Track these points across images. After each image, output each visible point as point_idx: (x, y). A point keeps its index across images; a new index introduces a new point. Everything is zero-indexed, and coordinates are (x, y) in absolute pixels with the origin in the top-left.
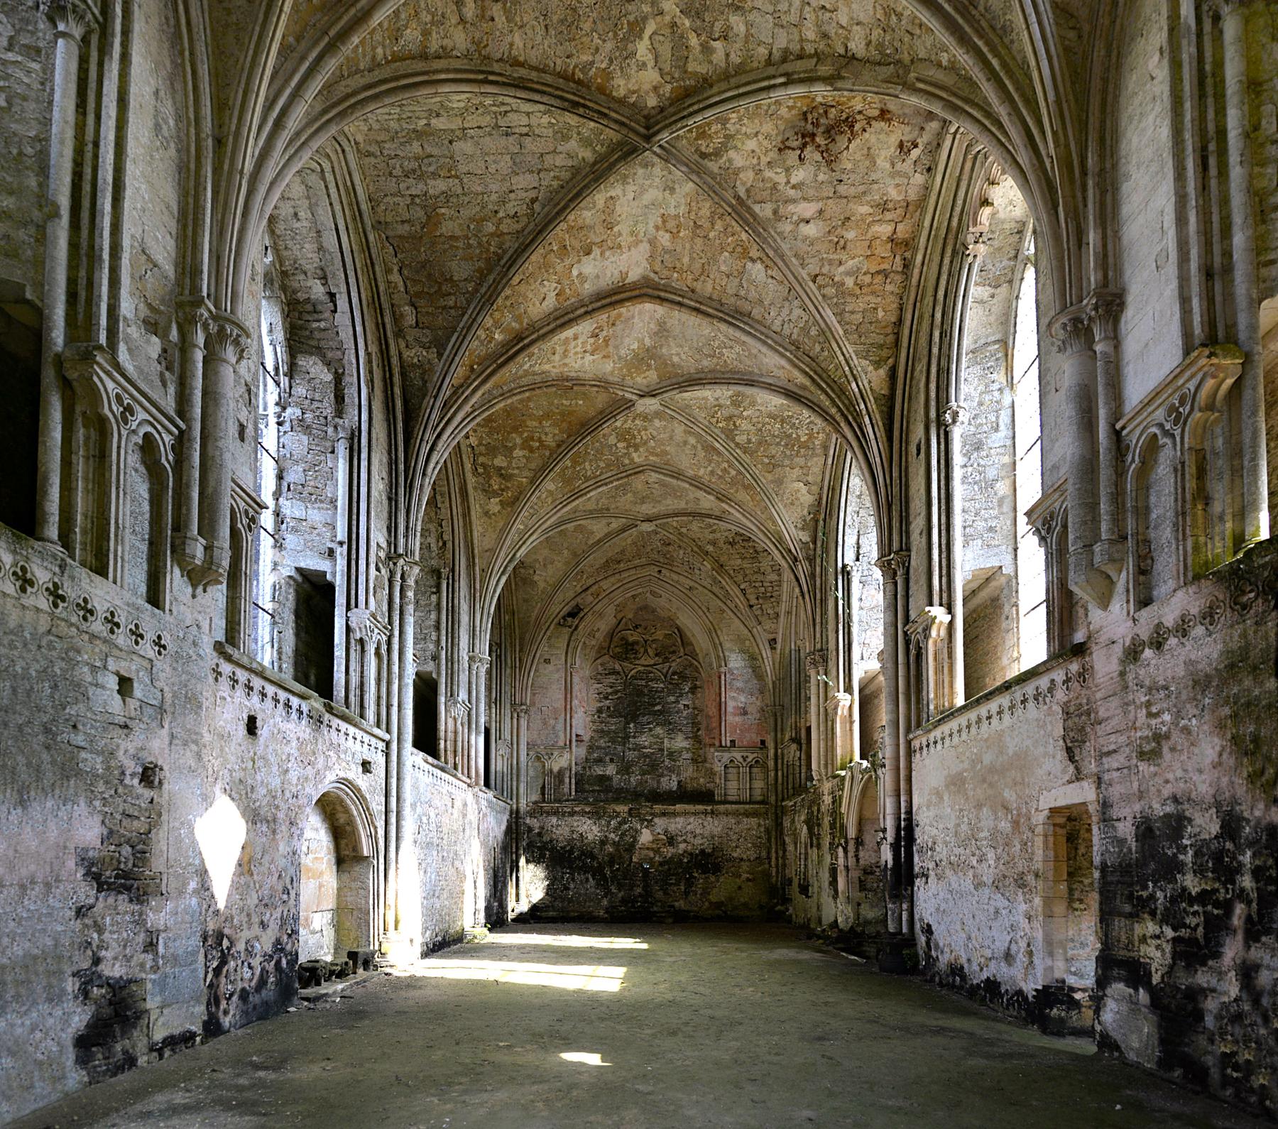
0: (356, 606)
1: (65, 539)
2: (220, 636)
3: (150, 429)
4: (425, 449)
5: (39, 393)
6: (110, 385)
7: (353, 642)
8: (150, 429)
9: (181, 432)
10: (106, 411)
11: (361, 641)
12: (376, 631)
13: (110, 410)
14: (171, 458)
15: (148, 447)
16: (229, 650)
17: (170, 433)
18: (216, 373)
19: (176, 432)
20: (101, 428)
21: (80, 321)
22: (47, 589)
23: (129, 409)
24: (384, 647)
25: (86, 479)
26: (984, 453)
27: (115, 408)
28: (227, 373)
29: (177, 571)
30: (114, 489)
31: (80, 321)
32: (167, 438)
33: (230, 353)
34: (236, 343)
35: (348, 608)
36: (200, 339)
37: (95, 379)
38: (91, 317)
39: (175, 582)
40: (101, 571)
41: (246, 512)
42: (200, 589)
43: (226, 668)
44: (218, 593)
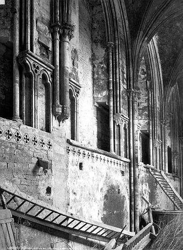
0: (117, 113)
1: (21, 116)
2: (69, 136)
3: (70, 88)
4: (138, 48)
5: (13, 71)
6: (32, 62)
7: (116, 126)
8: (70, 88)
9: (53, 70)
10: (31, 71)
11: (119, 126)
12: (124, 121)
13: (32, 70)
14: (51, 80)
15: (44, 77)
16: (71, 141)
17: (50, 71)
18: (63, 45)
19: (52, 70)
20: (29, 76)
21: (23, 46)
22: (16, 135)
23: (38, 68)
24: (127, 126)
25: (26, 94)
26: (125, 180)
27: (33, 69)
28: (67, 45)
29: (54, 118)
30: (34, 96)
31: (23, 46)
32: (49, 73)
33: (67, 39)
34: (69, 34)
35: (114, 114)
36: (58, 36)
37: (27, 62)
38: (26, 43)
39: (54, 123)
40: (31, 125)
41: (34, 65)
42: (61, 122)
43: (71, 148)
44: (68, 122)
